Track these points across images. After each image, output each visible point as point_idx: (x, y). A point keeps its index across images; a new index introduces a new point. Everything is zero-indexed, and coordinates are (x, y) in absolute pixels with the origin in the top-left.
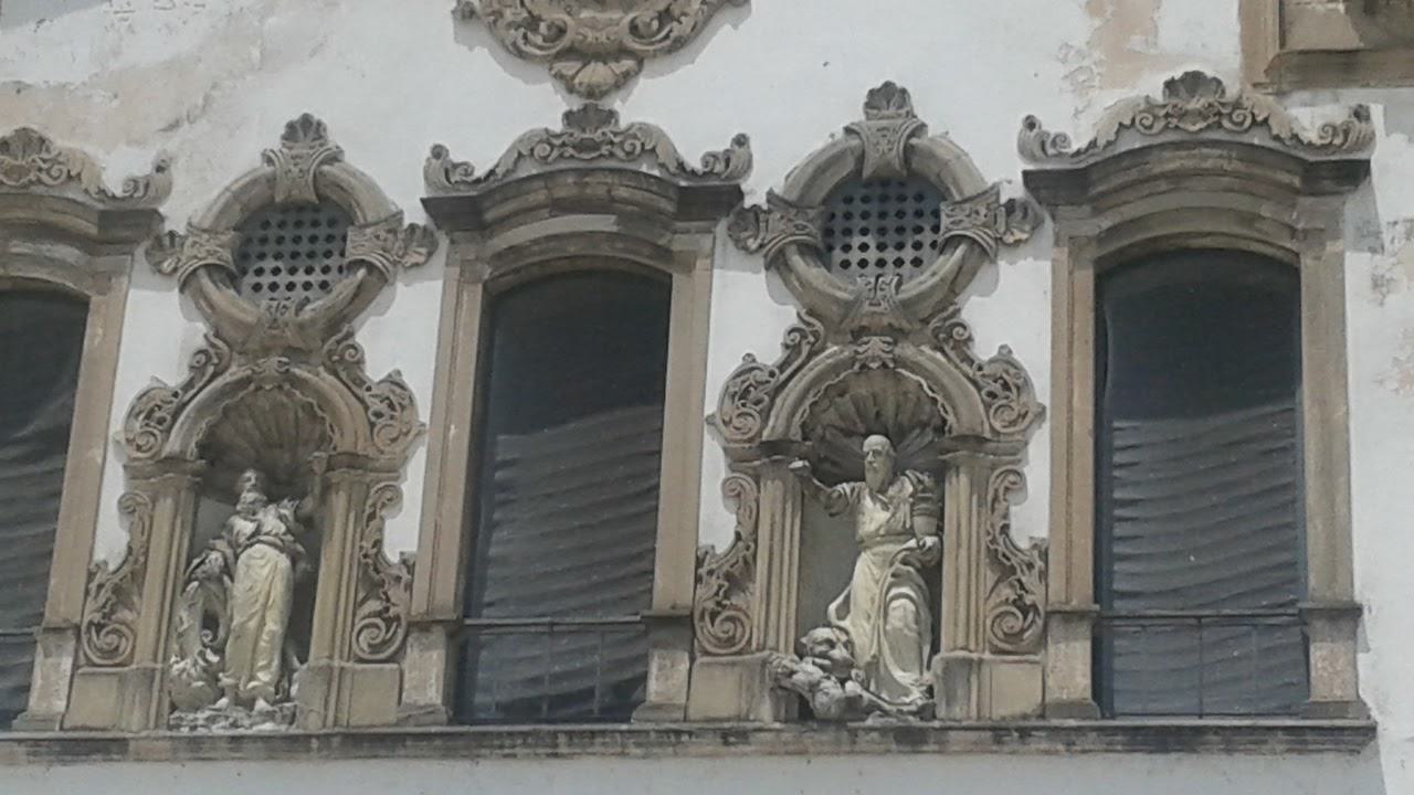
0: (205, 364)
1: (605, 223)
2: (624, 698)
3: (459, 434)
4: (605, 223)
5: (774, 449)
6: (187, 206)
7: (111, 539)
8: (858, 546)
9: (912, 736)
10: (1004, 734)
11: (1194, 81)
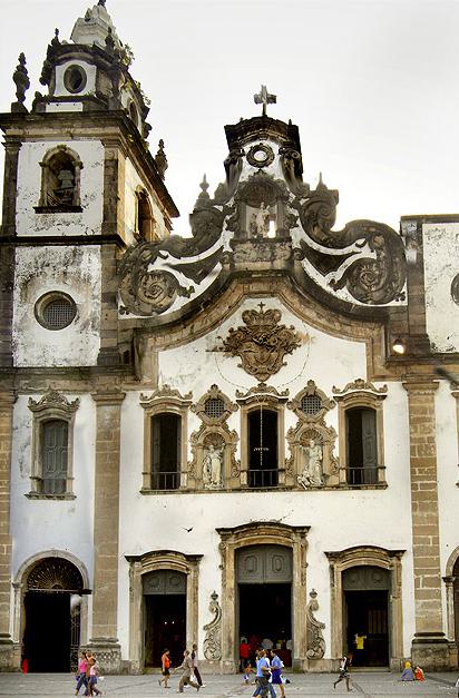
2: (275, 482)
6: (195, 400)
9: (319, 488)
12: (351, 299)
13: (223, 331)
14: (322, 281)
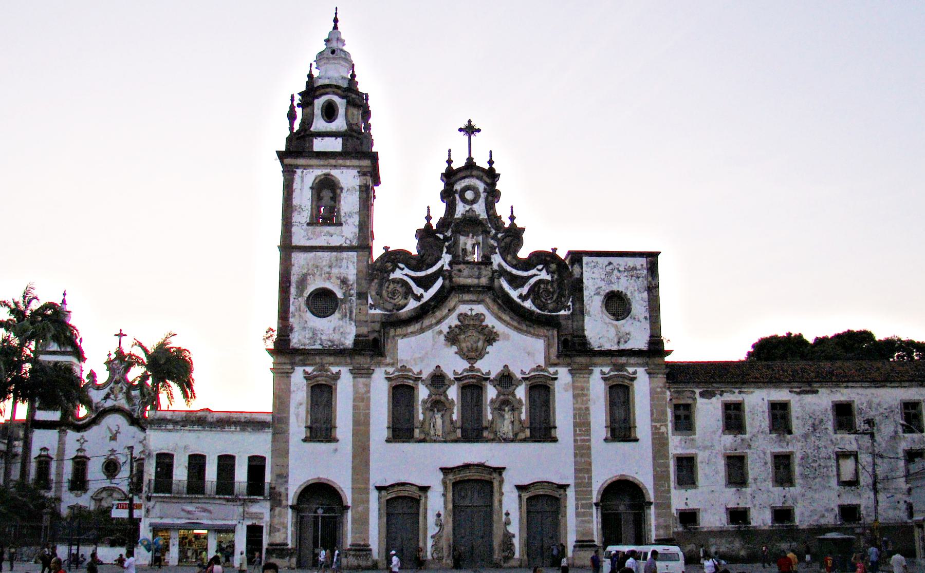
3: (460, 405)
7: (421, 417)
12: (534, 308)
13: (444, 327)
14: (514, 294)
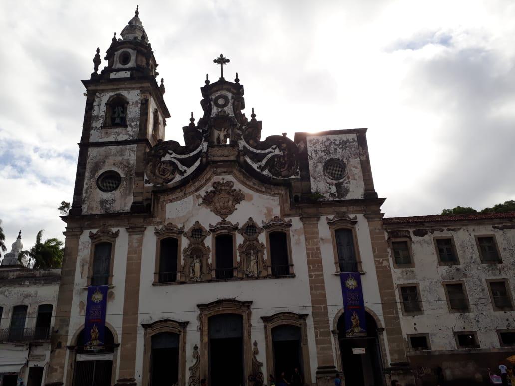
0: (190, 245)
1: (226, 231)
3: (214, 251)
4: (226, 231)
5: (243, 252)
7: (182, 262)
8: (250, 261)
9: (257, 278)
10: (265, 278)
11: (277, 217)
